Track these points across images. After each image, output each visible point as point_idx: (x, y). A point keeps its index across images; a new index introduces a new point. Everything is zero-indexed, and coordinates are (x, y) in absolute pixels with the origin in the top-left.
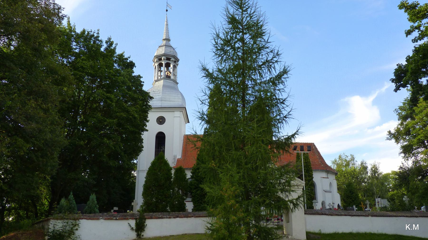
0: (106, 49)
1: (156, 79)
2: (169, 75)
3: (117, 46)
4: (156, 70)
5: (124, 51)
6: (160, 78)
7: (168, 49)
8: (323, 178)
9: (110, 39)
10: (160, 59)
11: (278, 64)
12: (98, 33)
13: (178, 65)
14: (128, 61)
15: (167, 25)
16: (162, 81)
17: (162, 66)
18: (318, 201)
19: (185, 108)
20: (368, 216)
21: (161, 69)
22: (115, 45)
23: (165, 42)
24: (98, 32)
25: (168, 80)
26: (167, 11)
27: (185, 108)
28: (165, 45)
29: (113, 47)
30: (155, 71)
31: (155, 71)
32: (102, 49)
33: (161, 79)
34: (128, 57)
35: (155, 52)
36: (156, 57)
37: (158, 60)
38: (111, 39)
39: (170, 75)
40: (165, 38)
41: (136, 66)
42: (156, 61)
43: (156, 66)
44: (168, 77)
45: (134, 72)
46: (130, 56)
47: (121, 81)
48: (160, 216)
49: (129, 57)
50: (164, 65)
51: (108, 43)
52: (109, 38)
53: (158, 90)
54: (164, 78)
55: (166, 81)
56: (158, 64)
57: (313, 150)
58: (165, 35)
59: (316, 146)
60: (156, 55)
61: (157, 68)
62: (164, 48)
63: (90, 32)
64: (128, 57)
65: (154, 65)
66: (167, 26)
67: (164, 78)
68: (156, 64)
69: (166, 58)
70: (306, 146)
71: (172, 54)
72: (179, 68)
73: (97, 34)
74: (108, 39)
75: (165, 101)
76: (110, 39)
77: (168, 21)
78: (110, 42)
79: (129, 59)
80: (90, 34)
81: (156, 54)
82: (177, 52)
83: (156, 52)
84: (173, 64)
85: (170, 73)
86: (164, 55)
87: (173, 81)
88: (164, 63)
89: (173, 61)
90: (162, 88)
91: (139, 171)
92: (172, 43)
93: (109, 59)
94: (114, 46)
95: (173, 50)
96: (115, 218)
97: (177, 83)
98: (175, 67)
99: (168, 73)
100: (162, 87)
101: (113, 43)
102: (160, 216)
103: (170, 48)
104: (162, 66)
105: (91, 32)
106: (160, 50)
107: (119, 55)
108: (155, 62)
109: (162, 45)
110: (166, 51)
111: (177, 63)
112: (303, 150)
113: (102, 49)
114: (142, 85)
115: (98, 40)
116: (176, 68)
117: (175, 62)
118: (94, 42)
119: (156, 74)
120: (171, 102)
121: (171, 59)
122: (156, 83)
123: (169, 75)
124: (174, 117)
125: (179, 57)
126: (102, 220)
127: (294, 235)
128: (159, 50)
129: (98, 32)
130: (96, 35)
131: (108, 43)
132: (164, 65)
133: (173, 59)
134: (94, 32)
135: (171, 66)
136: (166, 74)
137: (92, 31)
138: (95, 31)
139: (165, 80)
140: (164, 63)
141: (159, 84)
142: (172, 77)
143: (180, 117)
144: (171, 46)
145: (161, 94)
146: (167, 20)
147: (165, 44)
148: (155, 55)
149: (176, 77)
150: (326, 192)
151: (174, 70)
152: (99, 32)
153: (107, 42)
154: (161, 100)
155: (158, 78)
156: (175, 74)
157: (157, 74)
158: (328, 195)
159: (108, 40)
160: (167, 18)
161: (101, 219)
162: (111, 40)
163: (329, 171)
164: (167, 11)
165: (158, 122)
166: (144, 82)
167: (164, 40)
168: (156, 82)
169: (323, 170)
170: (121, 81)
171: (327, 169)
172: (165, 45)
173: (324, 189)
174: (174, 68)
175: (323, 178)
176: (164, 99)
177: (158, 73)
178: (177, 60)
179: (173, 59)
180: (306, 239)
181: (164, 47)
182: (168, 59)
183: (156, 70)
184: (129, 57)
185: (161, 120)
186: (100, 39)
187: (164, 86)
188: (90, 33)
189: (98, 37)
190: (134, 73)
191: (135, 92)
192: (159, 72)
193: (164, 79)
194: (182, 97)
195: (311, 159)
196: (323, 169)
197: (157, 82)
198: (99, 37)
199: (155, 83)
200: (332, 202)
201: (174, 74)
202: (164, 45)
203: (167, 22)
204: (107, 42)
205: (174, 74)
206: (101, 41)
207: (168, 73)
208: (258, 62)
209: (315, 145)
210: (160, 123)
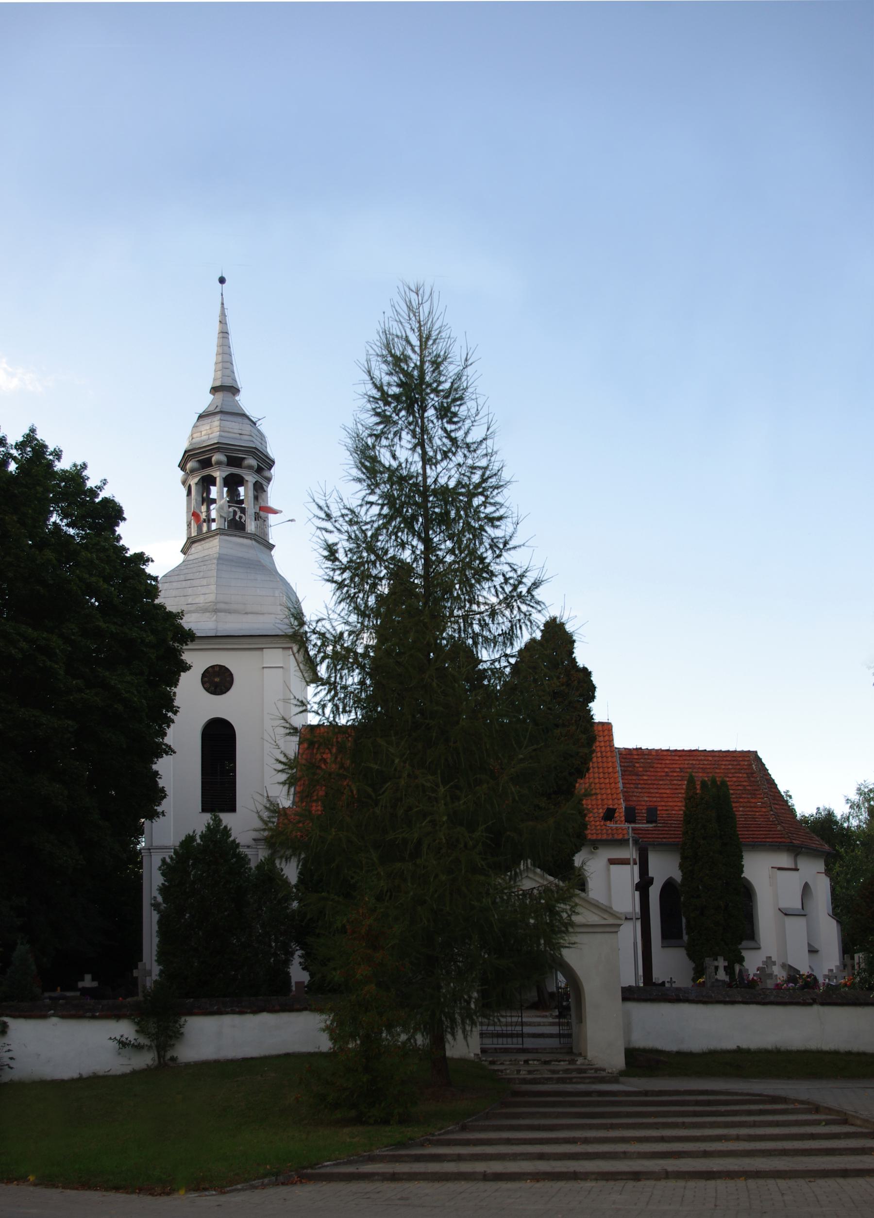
2: (241, 517)
8: (780, 869)
10: (206, 463)
11: (546, 580)
13: (269, 480)
14: (59, 988)
18: (762, 945)
20: (810, 1004)
25: (235, 536)
33: (211, 534)
34: (96, 487)
44: (236, 526)
48: (215, 1008)
50: (219, 481)
55: (227, 540)
56: (199, 480)
57: (753, 777)
59: (764, 761)
61: (197, 491)
67: (220, 532)
68: (193, 481)
70: (727, 763)
75: (229, 612)
77: (229, 320)
86: (218, 447)
87: (255, 539)
88: (219, 475)
91: (151, 851)
92: (246, 401)
96: (88, 1014)
97: (271, 547)
98: (260, 489)
102: (215, 1008)
103: (239, 419)
110: (223, 434)
111: (266, 473)
112: (634, 822)
116: (264, 493)
117: (259, 470)
120: (250, 616)
123: (241, 517)
124: (263, 668)
125: (272, 451)
126: (54, 1020)
127: (590, 1055)
132: (219, 481)
133: (252, 462)
140: (219, 475)
143: (282, 667)
144: (244, 415)
145: (213, 587)
147: (219, 404)
149: (265, 523)
150: (786, 914)
154: (216, 611)
158: (796, 926)
161: (53, 1015)
163: (802, 848)
165: (207, 685)
168: (194, 542)
169: (781, 842)
171: (794, 841)
173: (783, 905)
175: (780, 869)
176: (222, 606)
178: (265, 464)
180: (624, 1065)
181: (218, 417)
182: (234, 461)
185: (217, 680)
192: (205, 505)
195: (743, 807)
196: (780, 840)
200: (809, 945)
202: (218, 410)
208: (478, 596)
209: (758, 760)
210: (215, 688)
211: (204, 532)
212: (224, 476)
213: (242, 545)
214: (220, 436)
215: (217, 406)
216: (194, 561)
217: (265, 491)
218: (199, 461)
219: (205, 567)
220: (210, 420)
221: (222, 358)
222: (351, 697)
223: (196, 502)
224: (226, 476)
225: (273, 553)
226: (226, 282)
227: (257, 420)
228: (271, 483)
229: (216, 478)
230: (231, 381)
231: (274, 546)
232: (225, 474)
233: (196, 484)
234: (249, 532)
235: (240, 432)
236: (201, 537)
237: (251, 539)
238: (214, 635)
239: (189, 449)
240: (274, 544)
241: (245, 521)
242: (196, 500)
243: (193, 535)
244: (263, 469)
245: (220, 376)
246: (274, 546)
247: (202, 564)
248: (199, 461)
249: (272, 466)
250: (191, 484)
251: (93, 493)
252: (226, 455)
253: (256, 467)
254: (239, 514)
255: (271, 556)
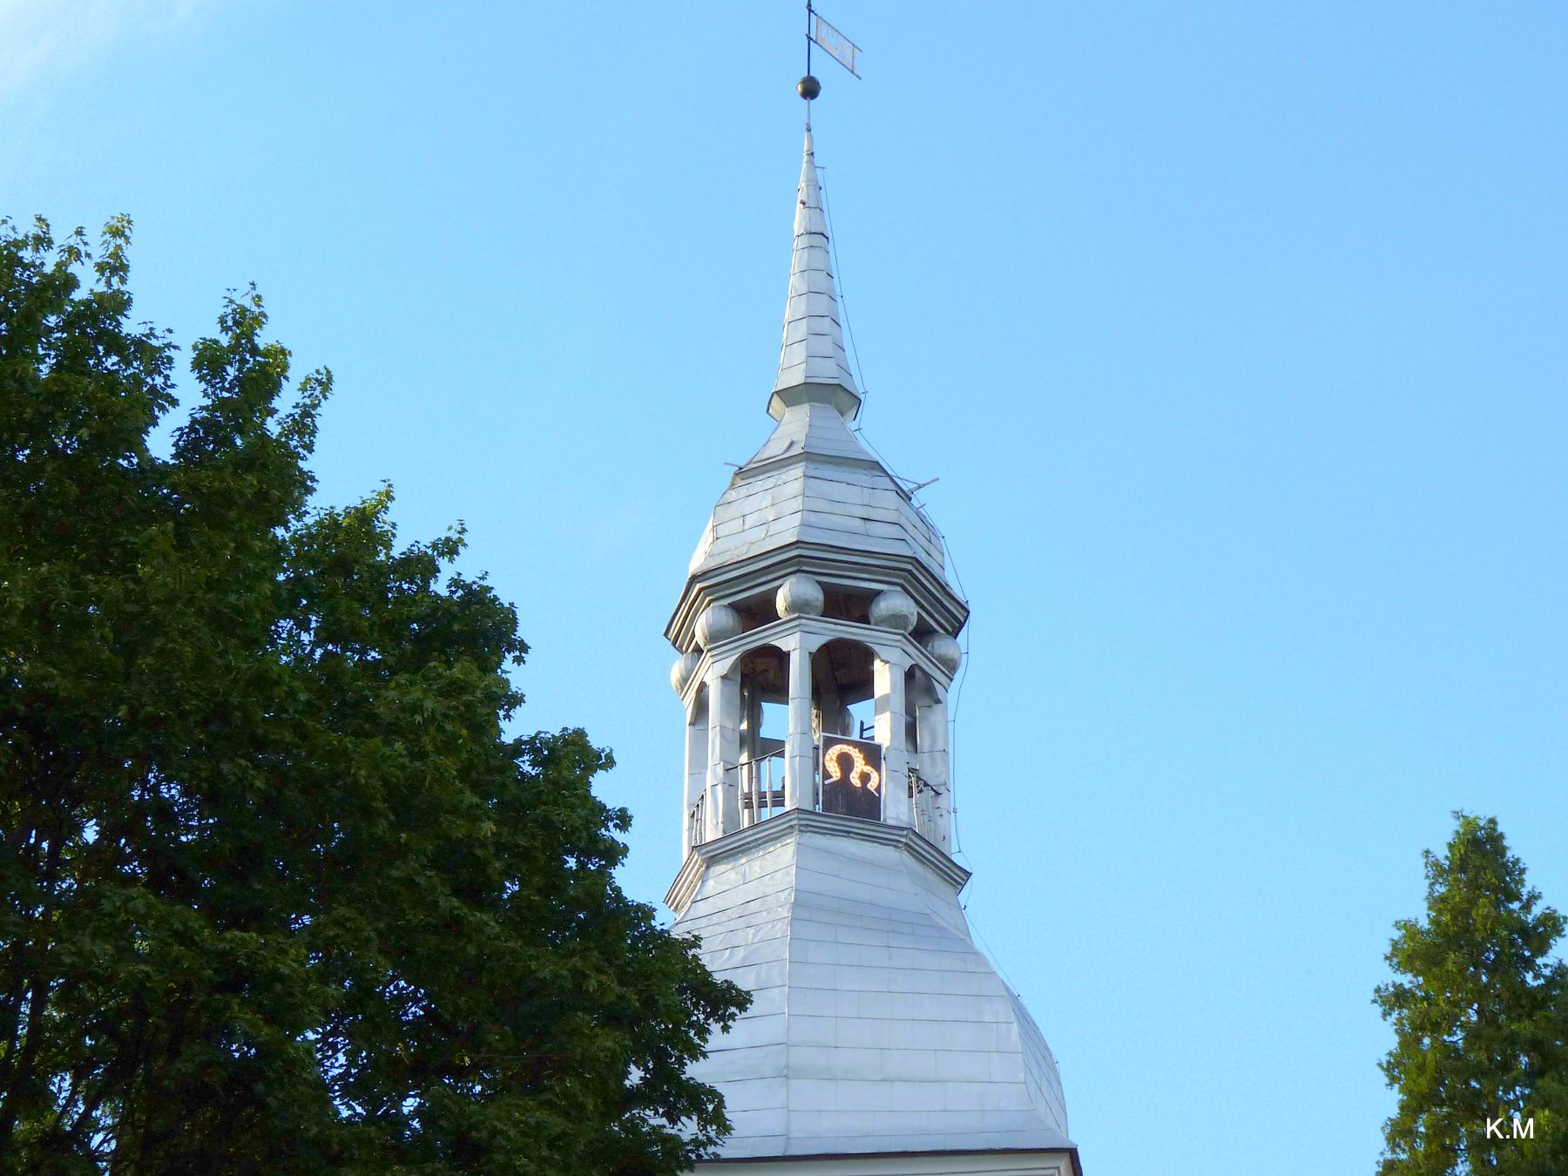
0: (192, 442)
1: (712, 833)
2: (865, 778)
3: (325, 408)
4: (714, 736)
5: (383, 488)
6: (751, 817)
7: (838, 491)
9: (244, 322)
10: (758, 612)
12: (115, 267)
13: (950, 667)
14: (440, 587)
15: (818, 236)
16: (784, 855)
17: (779, 693)
19: (1064, 1164)
21: (755, 719)
22: (298, 397)
23: (795, 424)
24: (116, 255)
26: (811, 89)
27: (1072, 1154)
28: (809, 456)
29: (281, 414)
30: (699, 745)
31: (699, 745)
32: (161, 443)
34: (434, 546)
35: (707, 523)
36: (707, 584)
37: (727, 619)
38: (259, 320)
39: (875, 776)
40: (795, 378)
41: (524, 648)
42: (714, 637)
43: (703, 686)
45: (516, 700)
46: (455, 536)
47: (385, 782)
49: (450, 548)
50: (798, 676)
51: (232, 372)
52: (244, 310)
53: (740, 953)
54: (805, 821)
58: (800, 352)
60: (712, 564)
62: (796, 487)
63: (21, 244)
64: (433, 538)
65: (685, 680)
66: (819, 253)
68: (714, 671)
69: (815, 594)
71: (881, 540)
72: (959, 695)
73: (101, 268)
74: (222, 320)
76: (244, 322)
78: (255, 351)
79: (443, 563)
80: (26, 267)
81: (710, 555)
82: (941, 526)
83: (708, 536)
84: (895, 655)
85: (873, 754)
89: (896, 621)
90: (782, 929)
93: (243, 547)
94: (287, 401)
95: (892, 500)
97: (957, 877)
99: (845, 762)
100: (791, 924)
101: (285, 367)
103: (861, 477)
104: (779, 693)
105: (42, 241)
106: (748, 506)
107: (331, 525)
108: (700, 638)
109: (776, 449)
110: (813, 518)
111: (942, 646)
113: (161, 443)
114: (614, 853)
115: (116, 344)
116: (937, 708)
117: (922, 634)
118: (73, 359)
119: (714, 773)
121: (883, 607)
122: (711, 883)
123: (865, 778)
125: (960, 578)
128: (735, 510)
129: (116, 255)
130: (88, 283)
131: (232, 372)
132: (798, 676)
133: (894, 603)
134: (74, 253)
135: (884, 678)
136: (827, 775)
137: (53, 235)
138: (79, 232)
139: (820, 840)
141: (752, 890)
142: (896, 808)
146: (816, 187)
148: (696, 564)
149: (942, 801)
151: (911, 731)
152: (131, 254)
153: (209, 361)
154: (786, 1074)
155: (730, 817)
156: (928, 774)
157: (720, 770)
159: (225, 329)
160: (811, 163)
162: (263, 339)
164: (811, 89)
166: (624, 820)
167: (789, 396)
168: (712, 861)
170: (385, 782)
172: (809, 456)
174: (910, 711)
177: (730, 769)
179: (894, 603)
181: (798, 471)
183: (714, 736)
184: (450, 548)
186: (131, 326)
187: (806, 906)
188: (27, 255)
189: (118, 304)
190: (517, 713)
191: (524, 919)
193: (805, 829)
194: (1021, 1026)
197: (717, 869)
198: (129, 302)
199: (704, 881)
201: (912, 770)
202: (796, 450)
203: (814, 206)
204: (209, 361)
205: (912, 770)
206: (150, 354)
207: (845, 762)
211: (746, 825)
212: (814, 649)
213: (870, 863)
214: (804, 525)
215: (792, 444)
216: (715, 919)
217: (938, 701)
218: (733, 607)
219: (752, 931)
220: (771, 482)
221: (808, 305)
222: (347, 1047)
223: (722, 736)
224: (821, 649)
225: (962, 898)
226: (816, 100)
227: (912, 486)
228: (958, 677)
229: (788, 654)
230: (834, 371)
231: (969, 874)
232: (816, 643)
233: (724, 678)
234: (890, 822)
235: (866, 513)
236: (735, 841)
237: (895, 844)
238: (780, 1154)
239: (705, 568)
240: (970, 871)
241: (878, 789)
242: (722, 728)
243: (709, 837)
244: (934, 631)
245: (802, 357)
246: (969, 874)
247: (741, 923)
248: (733, 607)
249: (962, 625)
250: (707, 680)
251: (420, 566)
252: (819, 582)
253: (914, 620)
254: (860, 765)
255: (962, 909)
